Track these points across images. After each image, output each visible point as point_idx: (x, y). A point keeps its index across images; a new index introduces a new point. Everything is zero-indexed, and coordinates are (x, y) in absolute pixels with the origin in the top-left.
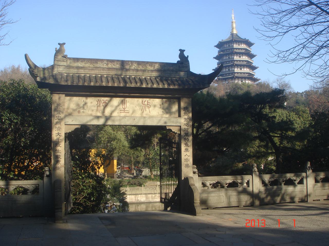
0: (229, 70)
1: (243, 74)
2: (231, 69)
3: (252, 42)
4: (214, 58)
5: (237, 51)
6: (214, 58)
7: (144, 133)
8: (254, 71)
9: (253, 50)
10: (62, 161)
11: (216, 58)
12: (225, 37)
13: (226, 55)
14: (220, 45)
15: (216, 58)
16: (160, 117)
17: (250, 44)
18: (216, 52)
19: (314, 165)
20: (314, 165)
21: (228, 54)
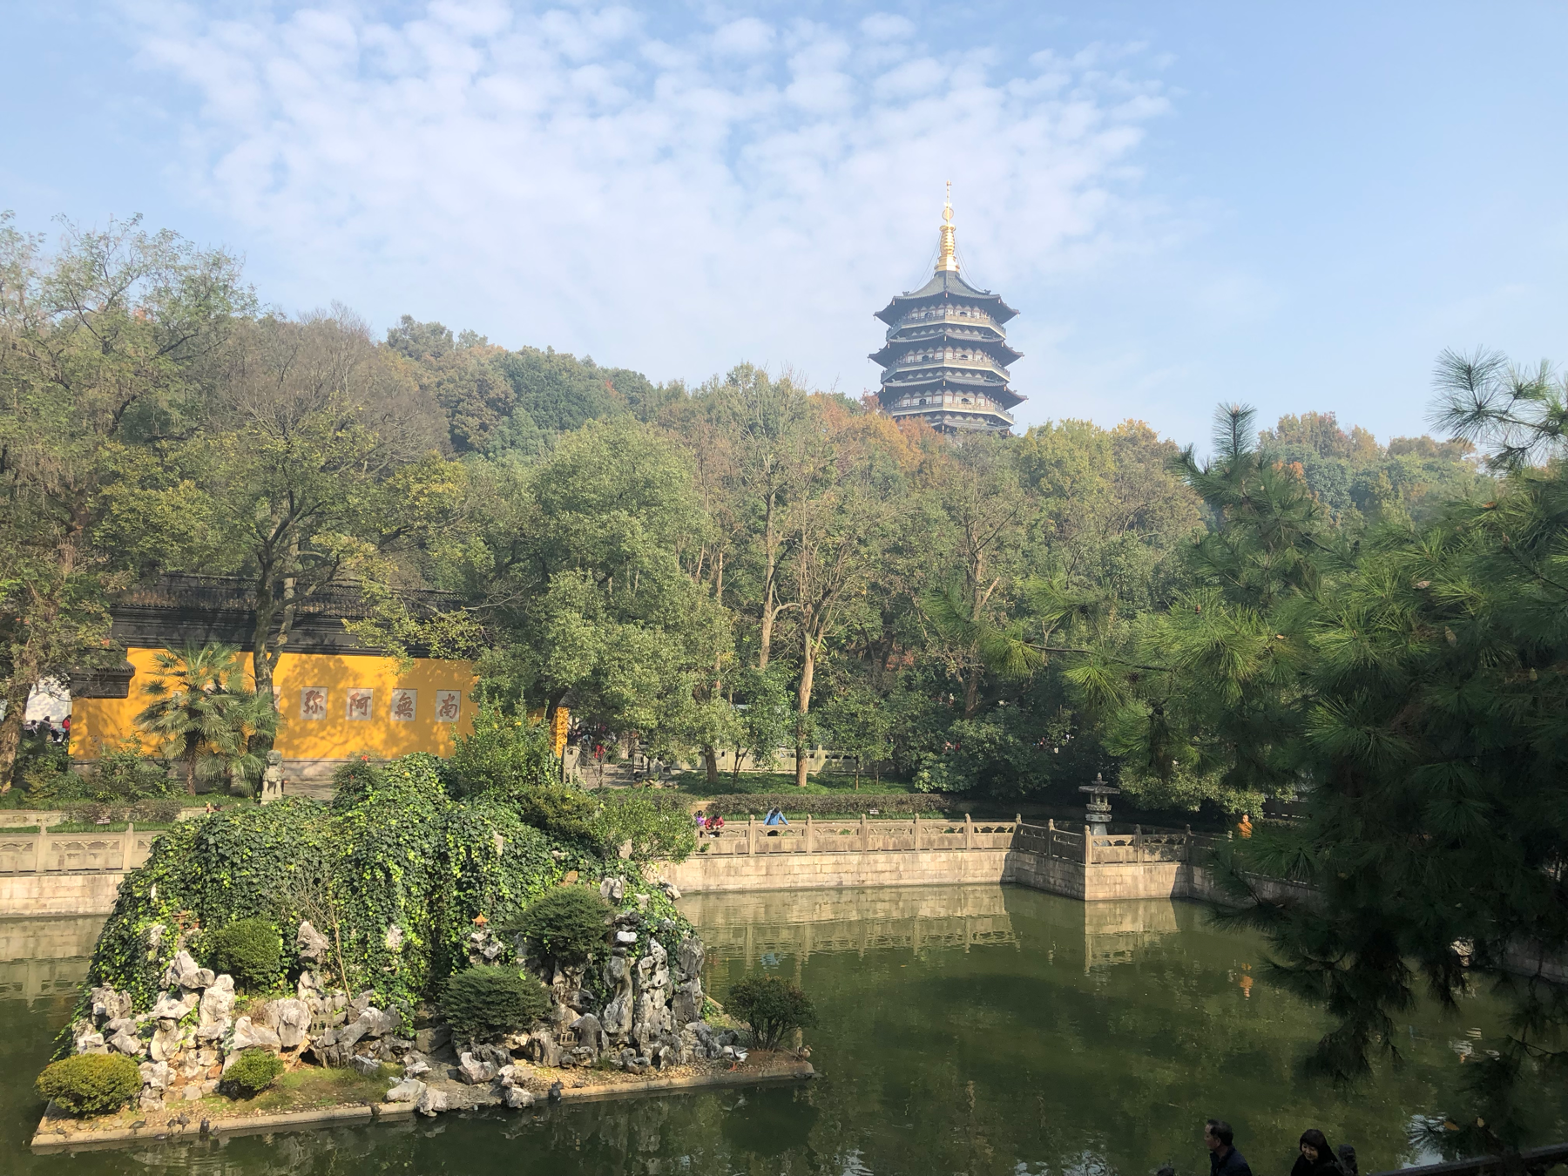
0: (923, 402)
1: (959, 418)
2: (928, 400)
3: (1011, 306)
4: (872, 357)
5: (958, 335)
6: (872, 357)
7: (92, 299)
8: (1010, 410)
9: (1012, 335)
10: (882, 868)
11: (879, 358)
12: (910, 278)
13: (915, 347)
14: (895, 312)
15: (879, 358)
16: (1094, 812)
17: (999, 311)
18: (878, 336)
19: (626, 936)
20: (626, 936)
21: (925, 345)
